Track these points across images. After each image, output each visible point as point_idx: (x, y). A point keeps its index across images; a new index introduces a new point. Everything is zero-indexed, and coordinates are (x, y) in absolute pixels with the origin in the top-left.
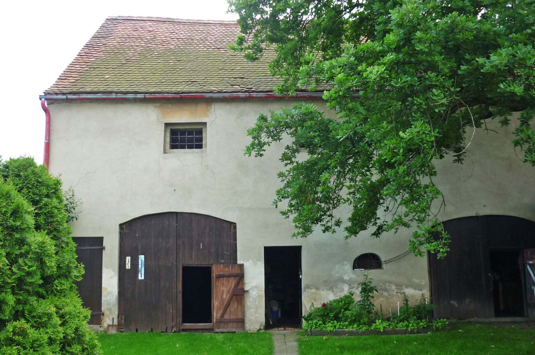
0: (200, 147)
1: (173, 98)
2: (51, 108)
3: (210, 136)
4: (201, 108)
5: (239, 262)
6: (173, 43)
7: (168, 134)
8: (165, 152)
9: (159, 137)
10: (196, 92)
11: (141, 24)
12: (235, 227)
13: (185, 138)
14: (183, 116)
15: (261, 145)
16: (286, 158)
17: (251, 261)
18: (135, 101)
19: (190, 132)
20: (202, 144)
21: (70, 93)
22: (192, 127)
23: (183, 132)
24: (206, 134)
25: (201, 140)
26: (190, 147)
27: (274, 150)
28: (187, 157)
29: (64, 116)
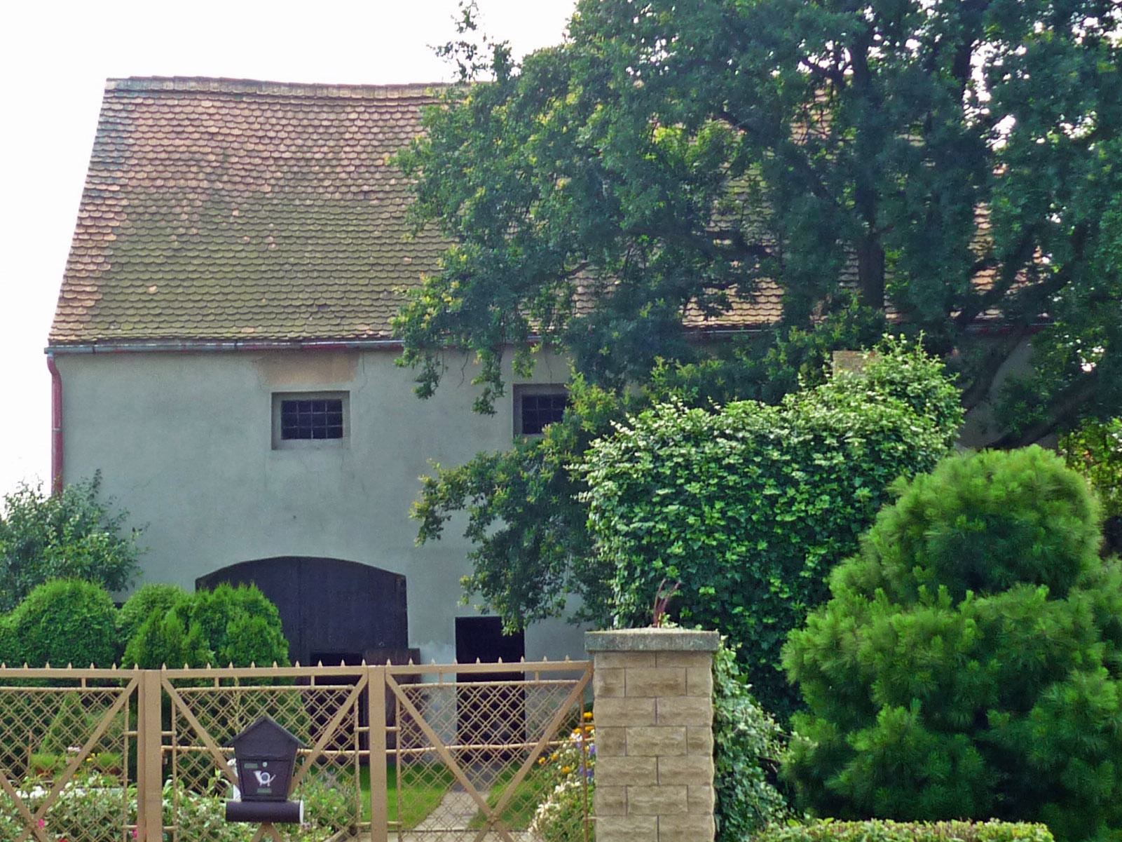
0: (337, 433)
1: (289, 350)
2: (60, 365)
3: (354, 416)
4: (338, 363)
5: (411, 646)
6: (268, 175)
7: (279, 412)
8: (274, 447)
9: (263, 419)
10: (330, 338)
11: (187, 107)
12: (404, 583)
13: (311, 420)
14: (305, 382)
15: (438, 521)
16: (473, 533)
17: (431, 643)
18: (218, 352)
19: (318, 405)
20: (341, 429)
21: (100, 341)
22: (322, 398)
23: (304, 405)
24: (349, 423)
25: (339, 420)
26: (320, 435)
27: (457, 521)
28: (312, 456)
29: (85, 377)
